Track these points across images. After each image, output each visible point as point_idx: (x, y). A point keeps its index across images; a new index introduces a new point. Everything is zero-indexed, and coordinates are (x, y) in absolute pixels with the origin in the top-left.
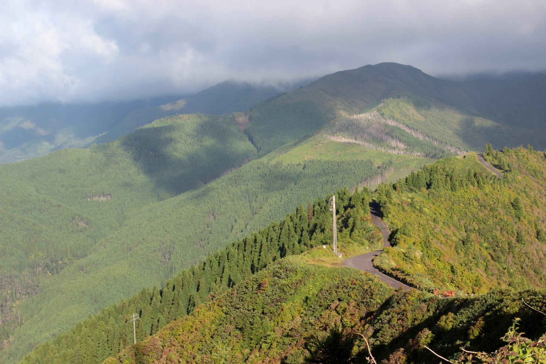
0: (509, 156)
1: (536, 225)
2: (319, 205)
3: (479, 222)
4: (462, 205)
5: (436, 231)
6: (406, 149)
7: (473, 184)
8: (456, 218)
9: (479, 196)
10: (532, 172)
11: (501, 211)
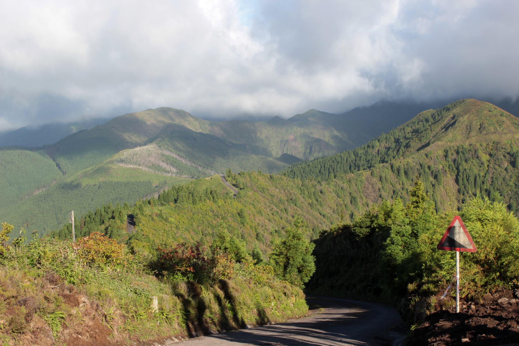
0: (244, 177)
1: (256, 229)
2: (89, 217)
3: (213, 228)
4: (200, 215)
5: (177, 235)
6: (177, 173)
7: (209, 199)
8: (195, 225)
9: (214, 208)
10: (261, 189)
11: (230, 219)
